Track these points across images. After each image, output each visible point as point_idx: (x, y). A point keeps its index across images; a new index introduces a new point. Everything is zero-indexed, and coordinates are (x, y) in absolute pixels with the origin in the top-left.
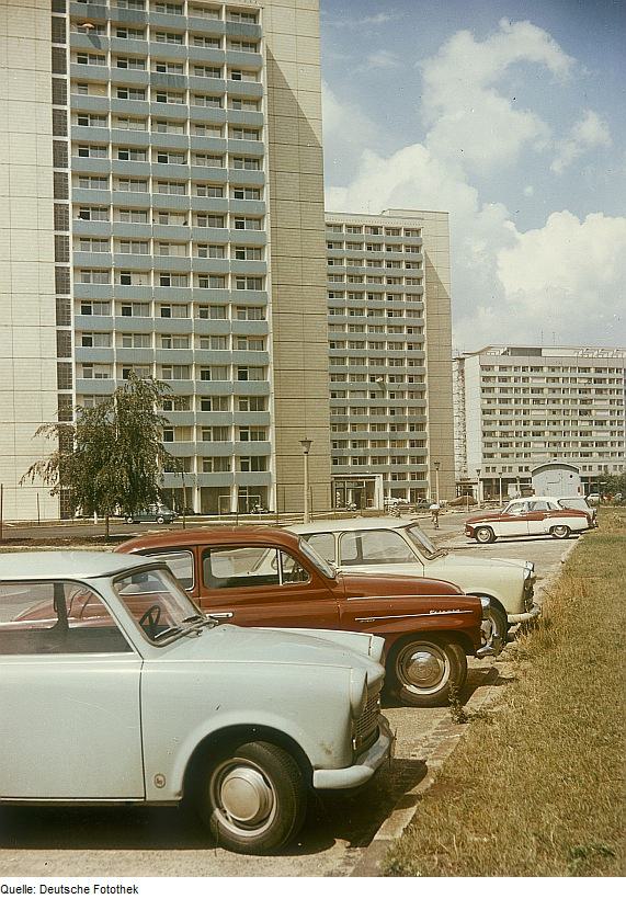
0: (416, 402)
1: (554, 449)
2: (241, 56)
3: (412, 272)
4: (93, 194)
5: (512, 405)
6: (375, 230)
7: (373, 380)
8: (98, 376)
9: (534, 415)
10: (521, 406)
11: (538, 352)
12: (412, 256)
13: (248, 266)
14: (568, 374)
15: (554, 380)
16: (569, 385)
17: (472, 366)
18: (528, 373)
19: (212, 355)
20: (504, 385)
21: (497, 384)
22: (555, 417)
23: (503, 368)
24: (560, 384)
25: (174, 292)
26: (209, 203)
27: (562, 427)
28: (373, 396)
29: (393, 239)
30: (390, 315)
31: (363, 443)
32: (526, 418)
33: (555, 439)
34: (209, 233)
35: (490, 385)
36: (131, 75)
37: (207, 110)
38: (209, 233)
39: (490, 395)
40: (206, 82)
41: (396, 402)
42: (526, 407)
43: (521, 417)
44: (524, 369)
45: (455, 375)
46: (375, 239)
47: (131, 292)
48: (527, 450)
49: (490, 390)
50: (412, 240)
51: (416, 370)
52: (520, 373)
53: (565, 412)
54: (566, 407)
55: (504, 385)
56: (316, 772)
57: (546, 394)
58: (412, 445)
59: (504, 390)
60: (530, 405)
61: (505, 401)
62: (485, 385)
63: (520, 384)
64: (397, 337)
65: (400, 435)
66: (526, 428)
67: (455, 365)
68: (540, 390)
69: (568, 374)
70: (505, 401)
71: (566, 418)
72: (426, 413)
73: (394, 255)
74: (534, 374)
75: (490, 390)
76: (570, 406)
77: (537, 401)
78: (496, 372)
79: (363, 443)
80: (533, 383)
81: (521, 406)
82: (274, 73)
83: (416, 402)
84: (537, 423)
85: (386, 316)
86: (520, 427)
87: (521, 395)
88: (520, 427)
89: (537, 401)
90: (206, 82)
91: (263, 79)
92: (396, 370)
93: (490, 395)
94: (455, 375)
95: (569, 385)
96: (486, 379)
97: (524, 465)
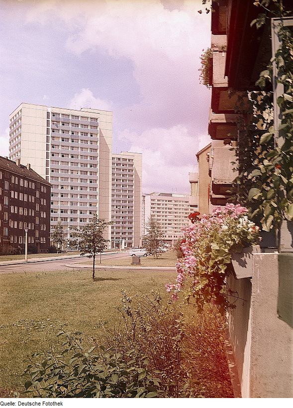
0: (130, 215)
1: (176, 230)
2: (93, 131)
3: (130, 173)
4: (55, 166)
5: (161, 214)
6: (119, 159)
7: (117, 207)
8: (55, 212)
9: (169, 217)
10: (164, 214)
11: (171, 195)
12: (130, 168)
13: (92, 185)
14: (181, 203)
15: (176, 205)
16: (181, 207)
17: (148, 199)
18: (167, 203)
19: (83, 208)
20: (158, 206)
21: (156, 206)
22: (176, 219)
23: (158, 200)
24: (178, 207)
25: (74, 191)
26: (84, 169)
27: (178, 222)
28: (117, 212)
29: (125, 162)
30: (123, 186)
31: (66, 211)
32: (166, 218)
33: (176, 226)
34: (83, 176)
35: (154, 206)
36: (65, 135)
37: (84, 145)
38: (83, 176)
39: (154, 210)
40: (84, 137)
41: (124, 214)
42: (166, 214)
43: (164, 218)
44: (166, 201)
45: (141, 201)
46: (119, 162)
47: (64, 191)
48: (166, 230)
49: (154, 208)
50: (130, 163)
51: (130, 204)
52: (164, 202)
53: (180, 217)
54: (180, 215)
55: (158, 206)
56: (226, 85)
57: (173, 210)
58: (128, 229)
59: (158, 208)
60: (168, 214)
61: (159, 212)
62: (152, 206)
63: (164, 206)
64: (125, 194)
65: (125, 225)
66: (166, 222)
67: (142, 198)
68: (171, 209)
69: (181, 203)
70: (159, 212)
71: (180, 219)
72: (133, 219)
73: (124, 167)
74: (169, 203)
75: (154, 208)
76: (181, 214)
77: (170, 212)
78: (156, 202)
79: (66, 211)
80: (168, 206)
81: (164, 214)
82: (101, 136)
83: (130, 215)
84: (170, 220)
85: (121, 186)
86: (164, 222)
87: (165, 210)
88: (164, 222)
89: (170, 212)
90: (84, 137)
91: (98, 137)
92: (124, 204)
93: (154, 210)
94: (141, 201)
95: (181, 207)
96: (152, 204)
97: (170, 235)
